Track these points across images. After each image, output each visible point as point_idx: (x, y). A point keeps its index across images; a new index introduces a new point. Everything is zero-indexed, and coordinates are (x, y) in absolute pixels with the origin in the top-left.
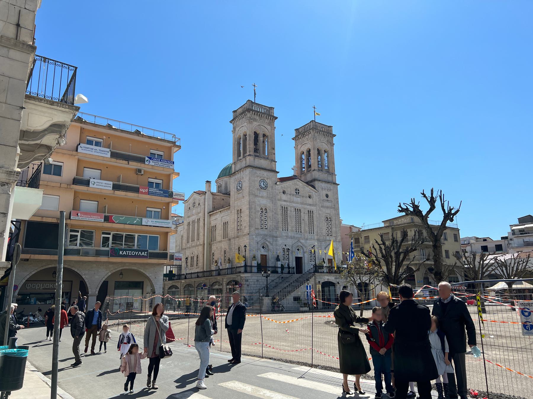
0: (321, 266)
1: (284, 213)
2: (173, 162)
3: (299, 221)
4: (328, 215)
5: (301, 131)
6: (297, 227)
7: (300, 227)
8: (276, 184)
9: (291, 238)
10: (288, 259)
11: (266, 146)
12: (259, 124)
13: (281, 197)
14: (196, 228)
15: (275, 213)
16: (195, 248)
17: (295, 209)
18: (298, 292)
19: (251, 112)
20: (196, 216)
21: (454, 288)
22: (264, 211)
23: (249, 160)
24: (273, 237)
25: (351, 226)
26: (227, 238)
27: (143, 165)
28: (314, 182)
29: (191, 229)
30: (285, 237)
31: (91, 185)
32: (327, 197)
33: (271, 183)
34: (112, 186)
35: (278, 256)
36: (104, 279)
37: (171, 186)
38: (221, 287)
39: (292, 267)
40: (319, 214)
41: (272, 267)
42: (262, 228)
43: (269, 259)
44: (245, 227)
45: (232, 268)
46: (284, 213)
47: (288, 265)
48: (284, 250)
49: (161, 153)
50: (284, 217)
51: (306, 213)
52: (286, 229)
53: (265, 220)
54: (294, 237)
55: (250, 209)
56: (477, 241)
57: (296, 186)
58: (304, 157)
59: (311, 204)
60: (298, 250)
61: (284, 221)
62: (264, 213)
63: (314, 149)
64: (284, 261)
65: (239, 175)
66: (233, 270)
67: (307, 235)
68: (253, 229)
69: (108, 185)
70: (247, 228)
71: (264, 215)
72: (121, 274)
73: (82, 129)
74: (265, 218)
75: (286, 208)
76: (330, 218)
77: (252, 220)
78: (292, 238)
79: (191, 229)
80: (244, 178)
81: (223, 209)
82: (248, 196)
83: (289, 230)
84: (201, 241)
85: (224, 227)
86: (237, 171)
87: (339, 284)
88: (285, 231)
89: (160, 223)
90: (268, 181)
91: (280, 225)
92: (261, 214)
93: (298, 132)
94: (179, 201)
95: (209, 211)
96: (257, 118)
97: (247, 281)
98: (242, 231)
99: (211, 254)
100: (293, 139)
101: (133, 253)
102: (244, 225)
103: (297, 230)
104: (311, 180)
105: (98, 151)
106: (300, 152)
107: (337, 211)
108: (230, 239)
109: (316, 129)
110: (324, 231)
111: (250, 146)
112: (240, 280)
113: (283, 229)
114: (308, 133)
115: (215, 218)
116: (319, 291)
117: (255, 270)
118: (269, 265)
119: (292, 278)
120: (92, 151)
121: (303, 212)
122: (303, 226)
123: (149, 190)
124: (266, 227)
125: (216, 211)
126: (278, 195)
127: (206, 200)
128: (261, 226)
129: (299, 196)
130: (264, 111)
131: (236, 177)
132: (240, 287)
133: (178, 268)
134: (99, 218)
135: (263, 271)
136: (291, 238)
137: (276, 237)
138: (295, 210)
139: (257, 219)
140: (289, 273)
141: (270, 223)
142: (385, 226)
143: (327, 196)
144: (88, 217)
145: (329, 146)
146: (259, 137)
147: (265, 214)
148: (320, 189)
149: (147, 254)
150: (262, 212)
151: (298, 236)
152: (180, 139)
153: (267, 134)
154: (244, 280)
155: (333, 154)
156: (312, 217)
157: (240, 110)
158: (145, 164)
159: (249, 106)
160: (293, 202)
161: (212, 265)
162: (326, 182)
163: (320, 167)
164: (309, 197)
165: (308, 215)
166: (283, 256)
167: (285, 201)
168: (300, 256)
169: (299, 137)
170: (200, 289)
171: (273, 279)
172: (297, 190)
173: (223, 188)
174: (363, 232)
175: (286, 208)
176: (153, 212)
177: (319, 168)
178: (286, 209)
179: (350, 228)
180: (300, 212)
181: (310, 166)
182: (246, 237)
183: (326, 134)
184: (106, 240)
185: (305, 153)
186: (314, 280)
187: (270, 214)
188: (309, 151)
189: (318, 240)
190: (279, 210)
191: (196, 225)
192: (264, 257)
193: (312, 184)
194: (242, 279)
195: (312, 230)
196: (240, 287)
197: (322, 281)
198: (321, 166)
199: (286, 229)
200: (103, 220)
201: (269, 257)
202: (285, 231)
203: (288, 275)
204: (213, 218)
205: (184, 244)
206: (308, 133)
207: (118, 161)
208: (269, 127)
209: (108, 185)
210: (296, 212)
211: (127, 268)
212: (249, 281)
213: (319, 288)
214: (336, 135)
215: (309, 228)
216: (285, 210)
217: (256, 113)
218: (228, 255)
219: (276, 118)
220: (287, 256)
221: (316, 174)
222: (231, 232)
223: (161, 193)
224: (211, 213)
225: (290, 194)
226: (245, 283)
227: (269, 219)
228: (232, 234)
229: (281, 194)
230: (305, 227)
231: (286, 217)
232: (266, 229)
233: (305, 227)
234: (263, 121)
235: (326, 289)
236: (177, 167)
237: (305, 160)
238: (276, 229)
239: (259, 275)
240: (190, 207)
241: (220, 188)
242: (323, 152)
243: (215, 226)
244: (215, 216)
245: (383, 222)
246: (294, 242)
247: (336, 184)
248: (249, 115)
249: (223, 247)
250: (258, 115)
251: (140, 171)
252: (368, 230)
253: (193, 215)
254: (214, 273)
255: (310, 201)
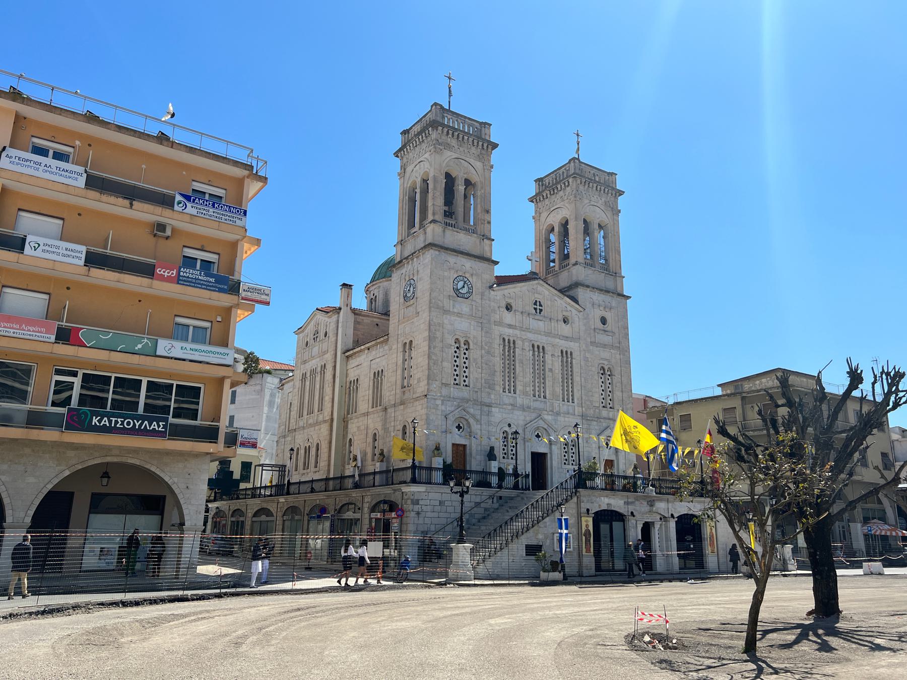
0: (592, 473)
1: (507, 354)
2: (245, 213)
3: (540, 373)
4: (606, 363)
5: (549, 183)
6: (537, 385)
7: (542, 385)
8: (491, 287)
9: (523, 408)
10: (514, 457)
11: (472, 207)
12: (455, 156)
13: (501, 318)
14: (318, 386)
15: (488, 352)
16: (313, 428)
17: (533, 346)
18: (537, 534)
19: (440, 128)
20: (318, 359)
21: (881, 532)
22: (462, 345)
23: (433, 232)
24: (483, 404)
25: (647, 396)
26: (380, 405)
27: (167, 212)
28: (576, 290)
29: (307, 388)
30: (510, 407)
31: (27, 250)
32: (604, 324)
33: (479, 285)
34: (83, 256)
35: (492, 449)
36: (50, 487)
37: (237, 268)
38: (358, 516)
39: (524, 473)
40: (586, 359)
41: (477, 472)
42: (457, 384)
43: (471, 454)
44: (419, 381)
45: (387, 472)
46: (507, 354)
47: (515, 469)
48: (505, 435)
49: (220, 192)
50: (507, 362)
51: (556, 354)
52: (512, 388)
53: (465, 366)
54: (529, 407)
55: (431, 339)
56: (903, 437)
57: (536, 296)
58: (553, 238)
59: (567, 337)
60: (538, 436)
61: (507, 370)
62: (462, 350)
63: (576, 219)
64: (505, 461)
65: (410, 266)
66: (389, 476)
67: (558, 405)
68: (435, 385)
69: (73, 254)
70: (424, 383)
71: (463, 355)
72: (106, 475)
73: (19, 119)
74: (465, 363)
75: (512, 342)
76: (609, 369)
77: (434, 364)
78: (524, 410)
79: (307, 388)
80: (421, 272)
81: (373, 343)
82: (427, 310)
83: (518, 392)
84: (326, 414)
85: (374, 383)
86: (407, 258)
87: (634, 516)
88: (510, 392)
89: (203, 354)
90: (474, 280)
91: (498, 378)
92: (456, 352)
93: (542, 185)
94: (257, 306)
95: (345, 349)
96: (454, 142)
97: (416, 502)
98: (411, 391)
99: (345, 442)
100: (531, 200)
101: (128, 424)
102: (417, 376)
103: (537, 393)
104: (568, 285)
105: (54, 170)
106: (545, 228)
107: (624, 355)
108: (386, 409)
109: (580, 176)
110: (597, 398)
111: (436, 201)
112: (400, 501)
113: (504, 388)
114: (563, 186)
115: (357, 363)
116: (588, 531)
117: (438, 476)
118: (471, 467)
119: (523, 499)
120: (38, 169)
121: (550, 353)
122: (549, 383)
123: (179, 271)
124: (467, 383)
125: (359, 348)
126: (494, 311)
127: (340, 325)
128: (455, 380)
129: (541, 318)
130: (469, 130)
131: (403, 271)
132: (400, 517)
133: (279, 471)
134: (41, 332)
135: (452, 479)
136: (523, 408)
137: (489, 406)
138: (531, 348)
139: (445, 364)
140: (516, 487)
141: (475, 374)
142: (725, 393)
143: (604, 321)
144: (13, 328)
145: (609, 214)
146: (456, 184)
147: (465, 354)
148: (589, 306)
149: (165, 427)
150: (457, 348)
151: (537, 405)
152: (266, 162)
153: (474, 178)
154: (409, 502)
155: (618, 232)
156: (570, 365)
157: (417, 128)
158: (173, 210)
159: (436, 115)
160: (528, 330)
161: (347, 467)
162: (601, 290)
163: (589, 257)
164: (565, 322)
165: (562, 361)
166: (504, 449)
167: (510, 326)
168: (542, 450)
169: (545, 195)
170: (314, 517)
171: (478, 500)
172: (538, 304)
173: (381, 301)
174: (677, 407)
175: (512, 342)
176: (191, 328)
177: (587, 261)
178: (512, 345)
179: (645, 400)
180: (544, 353)
181: (567, 257)
182: (421, 402)
183: (603, 188)
184: (62, 388)
185: (556, 229)
186: (574, 506)
187: (474, 353)
188: (565, 225)
189: (583, 416)
190: (496, 346)
191: (318, 379)
192: (460, 450)
193: (571, 293)
194: (405, 497)
195: (571, 394)
196: (400, 517)
197: (595, 509)
198: (591, 256)
199: (512, 388)
200: (53, 338)
201: (470, 449)
202: (510, 392)
203: (514, 493)
204: (353, 363)
205: (292, 421)
206: (563, 186)
207: (105, 198)
208: (478, 165)
209: (73, 254)
210: (534, 351)
211: (115, 460)
212: (421, 502)
213: (587, 526)
214: (624, 192)
215: (563, 390)
216: (509, 346)
217: (450, 132)
218: (380, 444)
219: (495, 146)
220: (512, 450)
221: (579, 273)
222: (389, 394)
223: (211, 282)
224: (348, 354)
225: (522, 313)
226: (411, 507)
227: (474, 364)
228: (391, 398)
229: (502, 310)
230: (554, 386)
231: (513, 363)
232: (466, 386)
233: (554, 386)
234: (466, 151)
235: (604, 528)
236: (253, 223)
237: (557, 243)
238: (489, 388)
239: (446, 489)
240: (307, 342)
241: (373, 305)
242: (596, 226)
243: (357, 380)
244: (358, 359)
245: (719, 386)
246: (528, 419)
247: (624, 296)
248: (434, 135)
249: (371, 426)
250: (455, 137)
251: (161, 227)
252: (689, 401)
253: (313, 358)
254: (349, 483)
255: (565, 329)
